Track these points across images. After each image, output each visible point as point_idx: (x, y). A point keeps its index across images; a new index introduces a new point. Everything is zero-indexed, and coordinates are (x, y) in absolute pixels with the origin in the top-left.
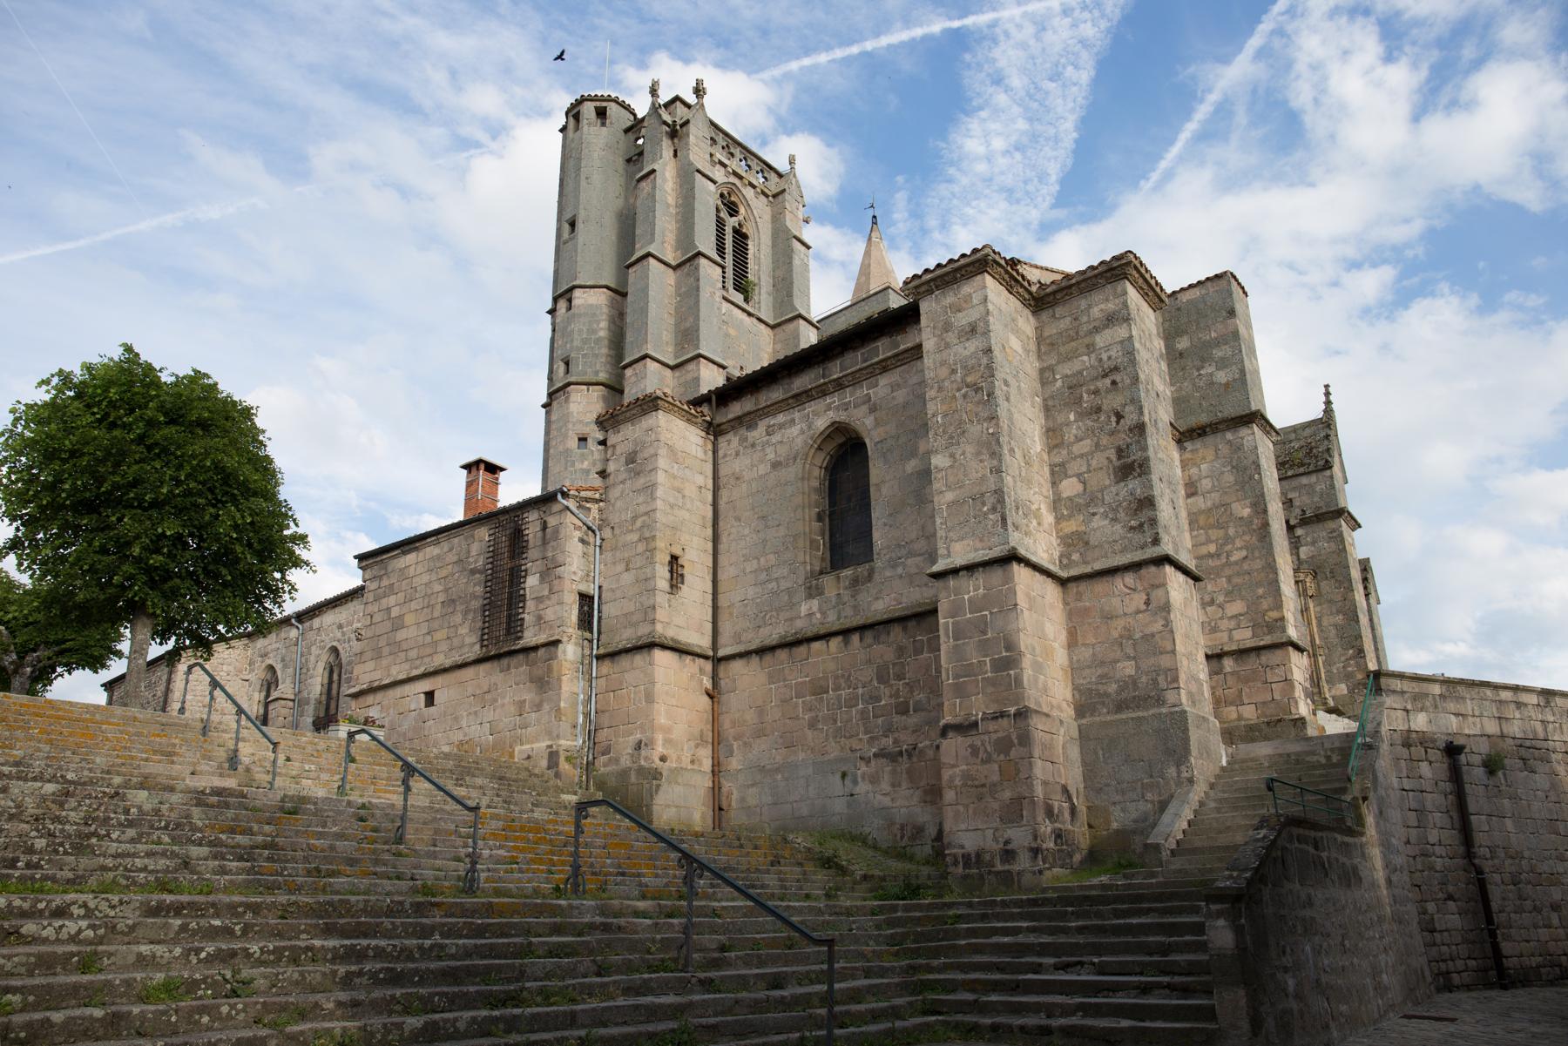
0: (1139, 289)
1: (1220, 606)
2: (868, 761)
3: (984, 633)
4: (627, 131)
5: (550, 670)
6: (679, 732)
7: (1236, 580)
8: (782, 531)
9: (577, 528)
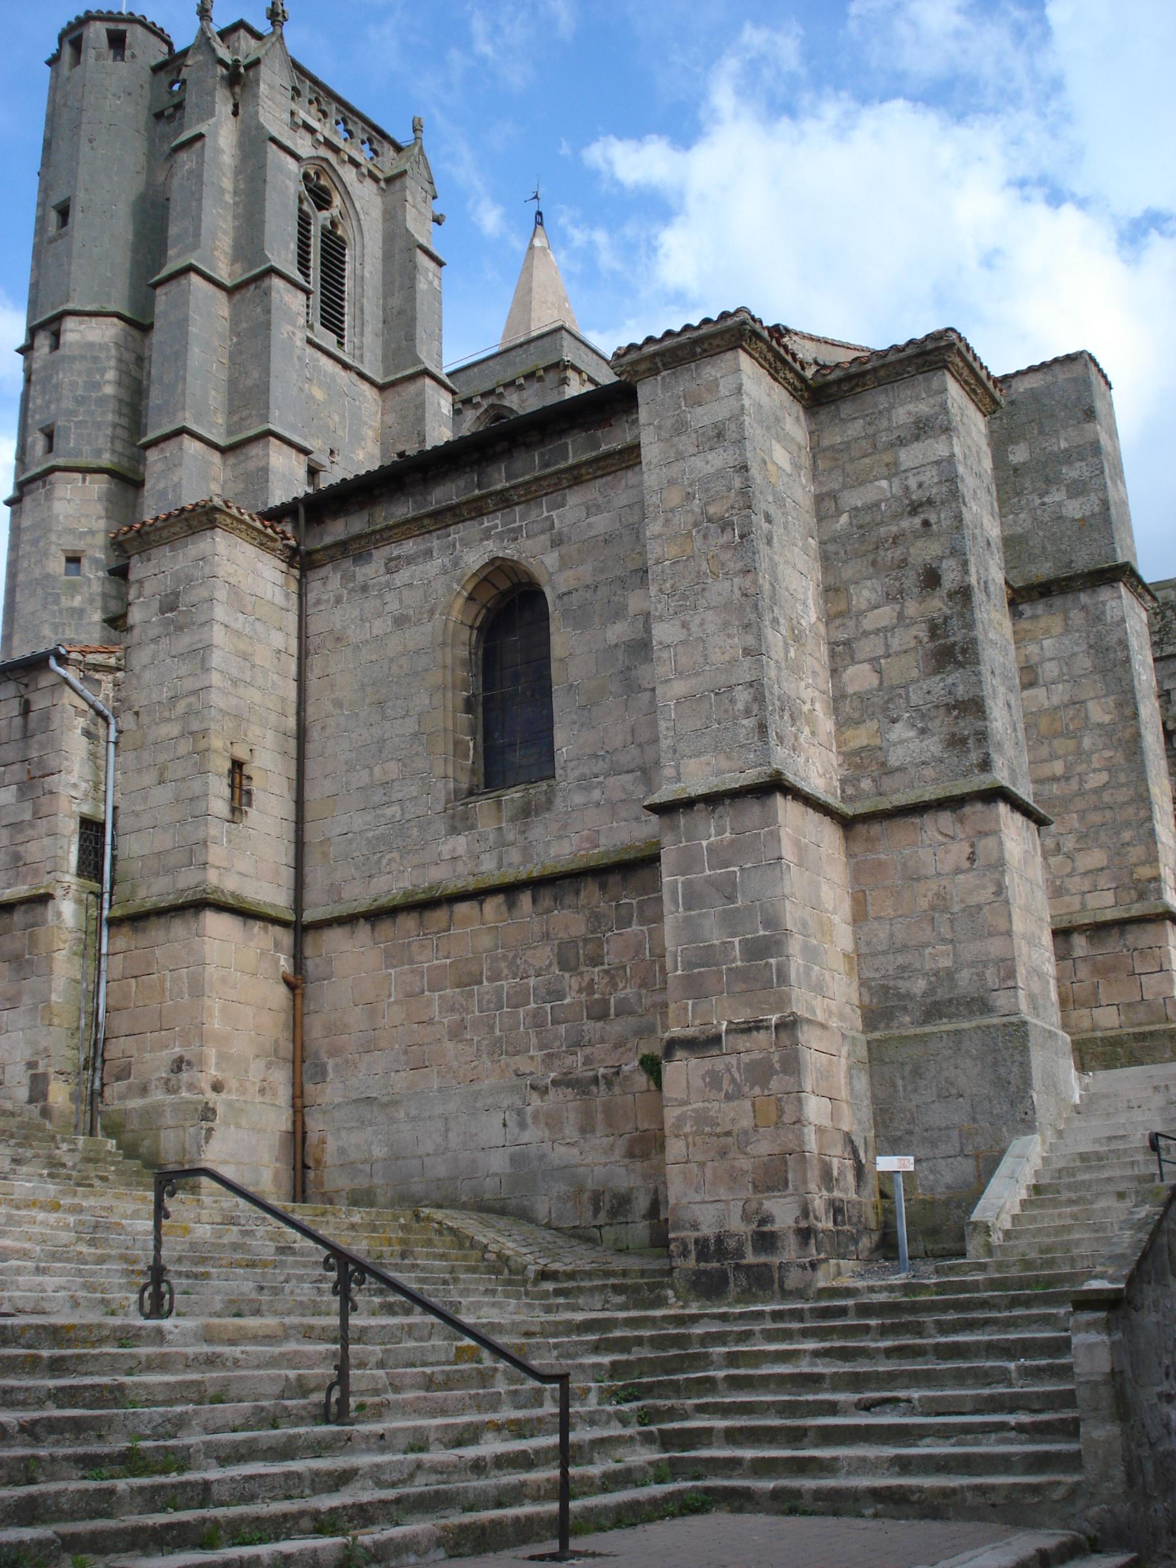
0: (963, 383)
1: (1069, 856)
2: (543, 1091)
3: (731, 898)
4: (156, 69)
5: (33, 941)
6: (242, 1046)
7: (1095, 818)
8: (411, 726)
9: (80, 713)
